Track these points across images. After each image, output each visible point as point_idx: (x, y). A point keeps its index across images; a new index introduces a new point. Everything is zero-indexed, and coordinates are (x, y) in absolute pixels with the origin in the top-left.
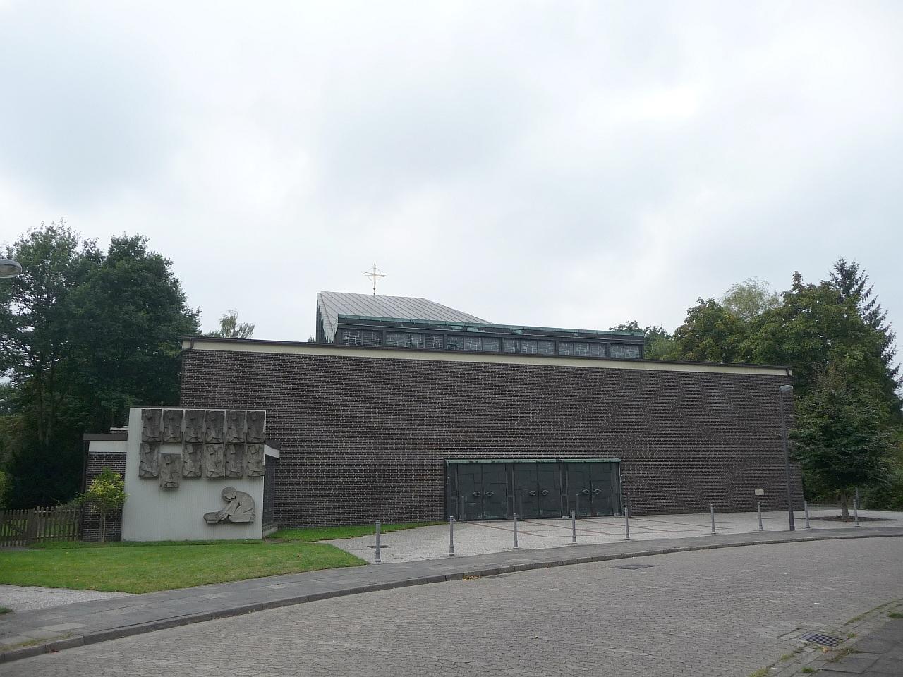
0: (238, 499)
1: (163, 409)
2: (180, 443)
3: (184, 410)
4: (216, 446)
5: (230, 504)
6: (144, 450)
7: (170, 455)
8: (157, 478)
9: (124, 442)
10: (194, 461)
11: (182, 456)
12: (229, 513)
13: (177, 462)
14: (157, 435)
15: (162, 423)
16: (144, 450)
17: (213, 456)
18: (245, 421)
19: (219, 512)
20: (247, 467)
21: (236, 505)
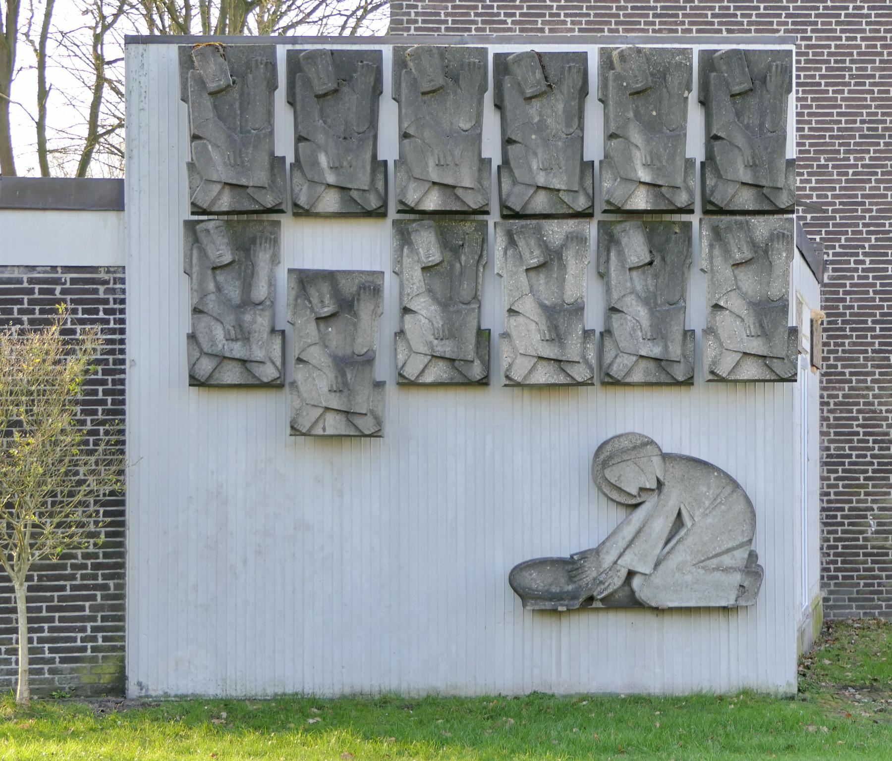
0: (673, 498)
1: (696, 48)
2: (380, 213)
3: (593, 52)
4: (556, 231)
5: (639, 515)
6: (727, 252)
7: (330, 276)
8: (275, 385)
9: (111, 217)
10: (446, 304)
11: (389, 284)
12: (629, 561)
13: (365, 309)
14: (260, 176)
15: (695, 118)
16: (727, 252)
17: (541, 280)
18: (281, 95)
19: (584, 555)
20: (710, 331)
21: (661, 526)
